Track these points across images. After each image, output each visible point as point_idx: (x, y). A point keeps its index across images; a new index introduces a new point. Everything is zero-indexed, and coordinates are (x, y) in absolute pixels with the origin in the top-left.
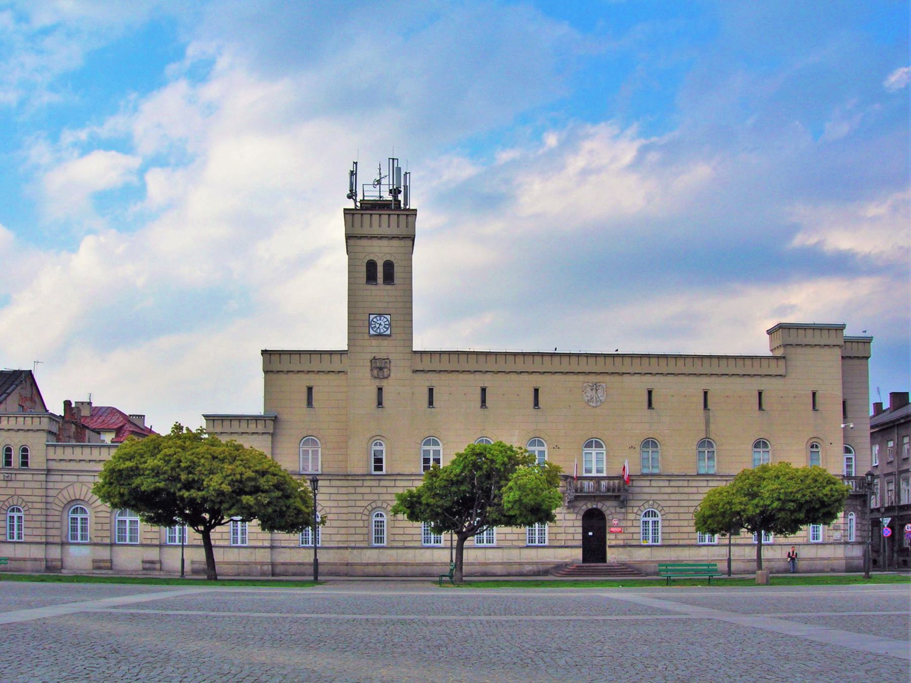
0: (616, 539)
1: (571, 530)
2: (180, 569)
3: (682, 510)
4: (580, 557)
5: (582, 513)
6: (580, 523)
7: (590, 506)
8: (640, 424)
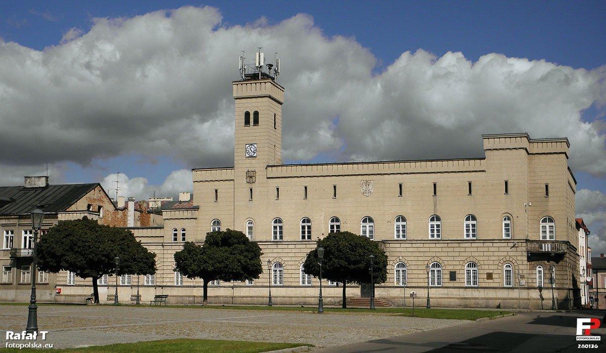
2: (342, 295)
3: (419, 263)
4: (359, 293)
8: (396, 207)
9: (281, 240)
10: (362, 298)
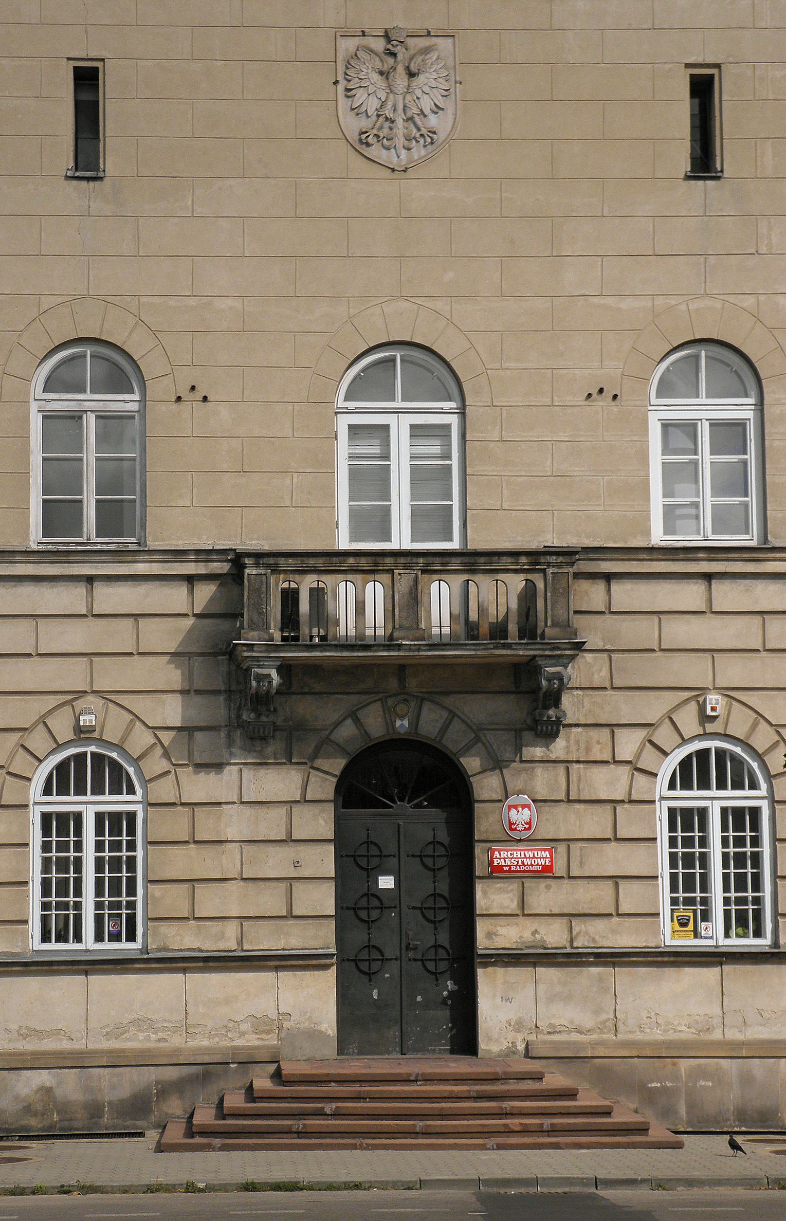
0: (523, 912)
1: (276, 862)
4: (328, 1022)
5: (337, 765)
6: (320, 822)
7: (375, 723)
9: (111, 543)
10: (356, 1066)
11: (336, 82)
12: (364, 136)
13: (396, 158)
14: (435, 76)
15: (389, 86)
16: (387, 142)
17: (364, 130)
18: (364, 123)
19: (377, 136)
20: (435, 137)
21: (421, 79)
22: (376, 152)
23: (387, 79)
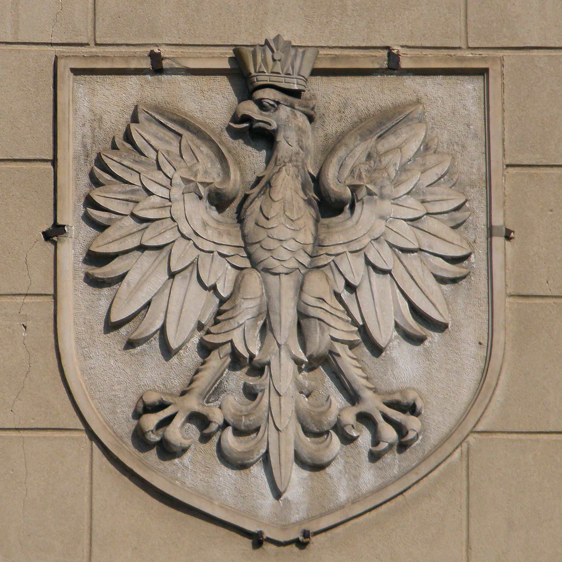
11: (54, 234)
12: (151, 421)
13: (268, 499)
14: (413, 208)
15: (247, 245)
16: (235, 443)
17: (153, 398)
18: (154, 375)
19: (200, 420)
20: (412, 423)
21: (364, 221)
22: (195, 474)
23: (240, 220)
